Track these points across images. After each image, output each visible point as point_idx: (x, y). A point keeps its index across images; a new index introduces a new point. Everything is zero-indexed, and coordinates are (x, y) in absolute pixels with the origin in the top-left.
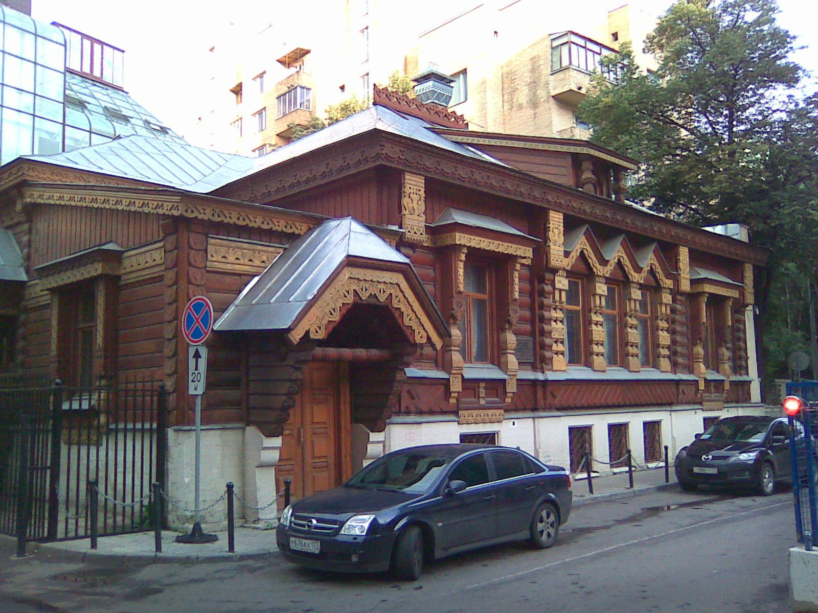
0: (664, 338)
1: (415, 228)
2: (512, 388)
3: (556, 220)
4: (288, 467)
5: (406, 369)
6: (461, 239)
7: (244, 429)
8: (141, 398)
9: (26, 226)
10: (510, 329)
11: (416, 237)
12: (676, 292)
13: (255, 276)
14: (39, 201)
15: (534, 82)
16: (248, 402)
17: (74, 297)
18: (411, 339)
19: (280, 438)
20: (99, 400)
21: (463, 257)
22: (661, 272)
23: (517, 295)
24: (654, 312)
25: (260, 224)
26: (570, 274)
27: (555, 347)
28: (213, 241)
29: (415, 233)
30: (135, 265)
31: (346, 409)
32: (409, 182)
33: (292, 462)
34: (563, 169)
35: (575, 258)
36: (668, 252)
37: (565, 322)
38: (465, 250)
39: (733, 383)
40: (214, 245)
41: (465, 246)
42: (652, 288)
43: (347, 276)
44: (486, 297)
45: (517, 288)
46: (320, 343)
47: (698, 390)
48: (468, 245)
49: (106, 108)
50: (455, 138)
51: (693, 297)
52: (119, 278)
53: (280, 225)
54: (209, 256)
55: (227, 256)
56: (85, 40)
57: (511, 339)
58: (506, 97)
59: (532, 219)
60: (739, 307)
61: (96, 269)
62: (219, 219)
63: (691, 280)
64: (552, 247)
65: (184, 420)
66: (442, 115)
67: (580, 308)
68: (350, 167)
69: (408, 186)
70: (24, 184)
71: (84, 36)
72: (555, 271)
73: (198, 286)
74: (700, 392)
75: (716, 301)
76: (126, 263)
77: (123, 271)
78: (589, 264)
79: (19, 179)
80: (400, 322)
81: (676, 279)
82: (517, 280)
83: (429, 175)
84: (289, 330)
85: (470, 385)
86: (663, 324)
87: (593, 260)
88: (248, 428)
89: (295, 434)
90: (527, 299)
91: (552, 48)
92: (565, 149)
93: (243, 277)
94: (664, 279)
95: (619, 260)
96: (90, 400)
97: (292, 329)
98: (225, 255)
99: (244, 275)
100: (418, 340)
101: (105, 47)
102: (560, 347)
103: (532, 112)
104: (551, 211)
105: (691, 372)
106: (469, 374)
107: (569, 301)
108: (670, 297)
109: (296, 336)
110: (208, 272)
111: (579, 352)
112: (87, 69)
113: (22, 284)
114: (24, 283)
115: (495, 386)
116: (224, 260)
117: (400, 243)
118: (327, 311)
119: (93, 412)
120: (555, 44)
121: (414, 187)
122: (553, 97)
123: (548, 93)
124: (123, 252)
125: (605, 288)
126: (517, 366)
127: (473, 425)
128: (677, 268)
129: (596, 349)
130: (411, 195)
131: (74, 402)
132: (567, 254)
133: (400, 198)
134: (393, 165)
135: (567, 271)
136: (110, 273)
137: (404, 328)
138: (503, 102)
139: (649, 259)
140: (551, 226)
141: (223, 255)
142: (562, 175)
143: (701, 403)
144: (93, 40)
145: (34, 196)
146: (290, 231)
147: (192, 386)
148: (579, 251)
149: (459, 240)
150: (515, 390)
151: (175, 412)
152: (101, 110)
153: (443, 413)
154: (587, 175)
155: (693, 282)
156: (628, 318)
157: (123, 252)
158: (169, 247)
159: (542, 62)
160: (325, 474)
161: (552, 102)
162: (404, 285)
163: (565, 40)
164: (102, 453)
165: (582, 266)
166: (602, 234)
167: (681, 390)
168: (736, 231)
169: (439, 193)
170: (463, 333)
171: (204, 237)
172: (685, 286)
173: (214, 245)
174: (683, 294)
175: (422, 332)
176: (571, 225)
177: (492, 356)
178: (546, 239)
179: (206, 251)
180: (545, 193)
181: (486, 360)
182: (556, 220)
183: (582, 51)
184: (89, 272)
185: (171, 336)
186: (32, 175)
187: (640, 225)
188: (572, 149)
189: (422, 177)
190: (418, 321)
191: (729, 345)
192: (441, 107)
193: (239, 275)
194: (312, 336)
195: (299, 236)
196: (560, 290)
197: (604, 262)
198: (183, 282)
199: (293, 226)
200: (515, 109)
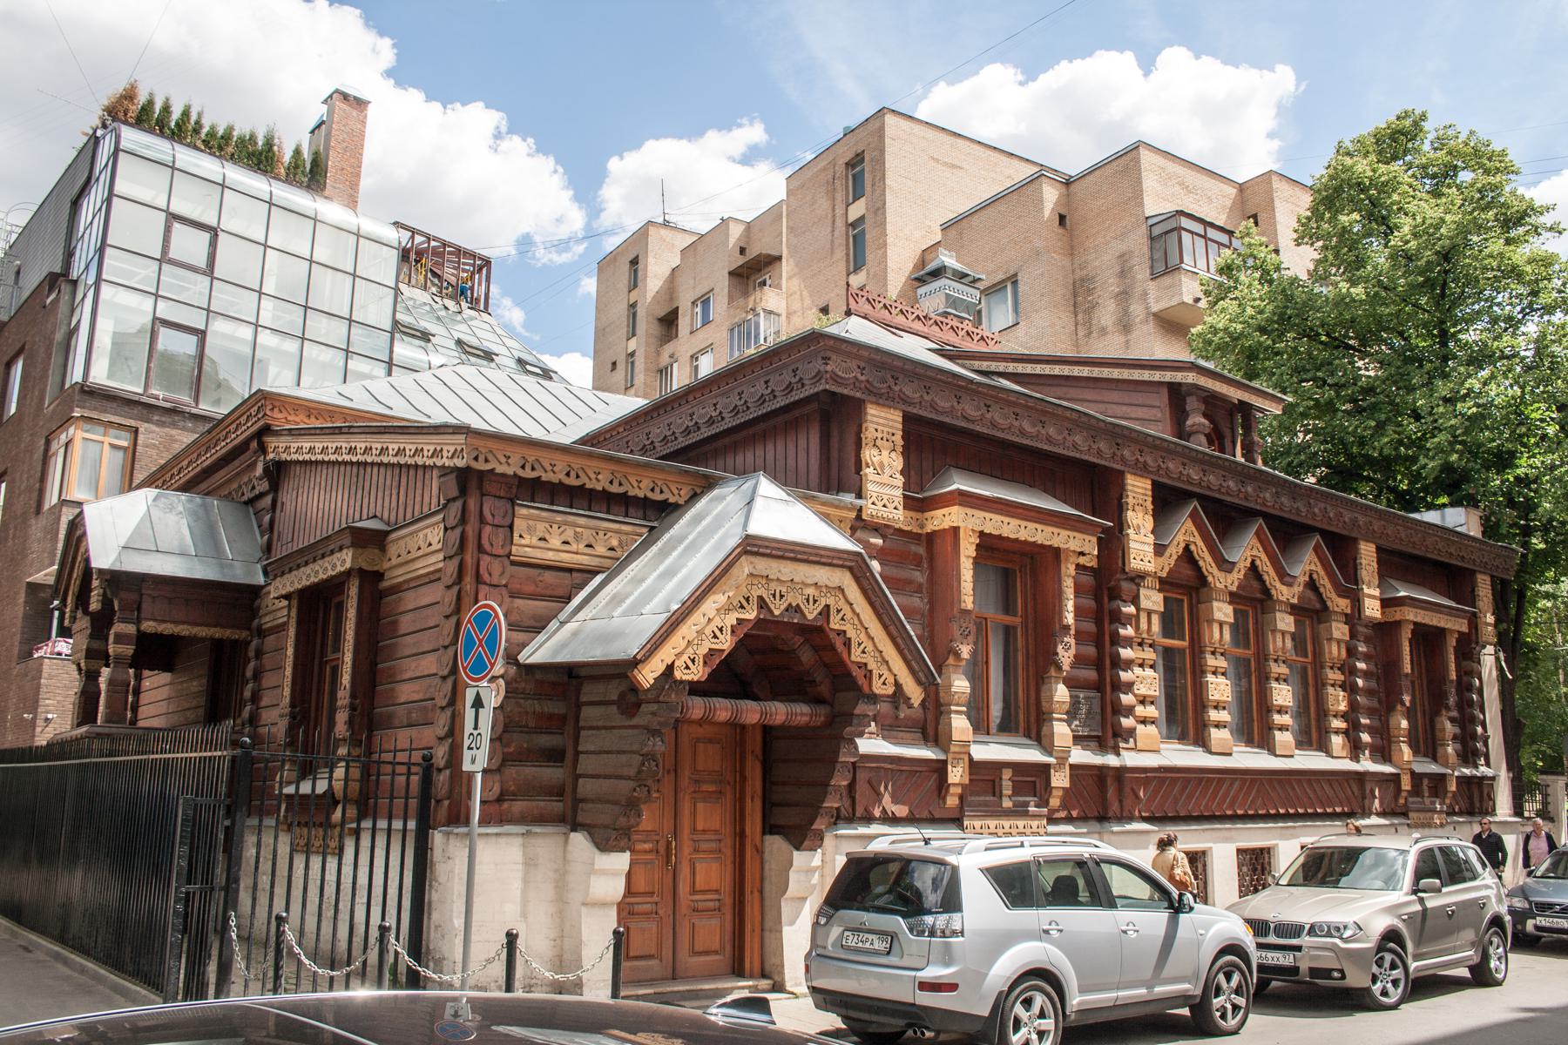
0: (1338, 701)
2: (1060, 780)
3: (1138, 489)
4: (647, 907)
5: (858, 741)
7: (566, 835)
8: (404, 778)
9: (268, 500)
12: (1354, 618)
13: (598, 573)
14: (284, 456)
15: (1125, 292)
17: (317, 605)
18: (866, 689)
19: (628, 854)
20: (346, 779)
22: (1329, 586)
23: (1070, 618)
24: (1318, 654)
26: (1165, 584)
27: (1140, 710)
28: (524, 511)
30: (404, 553)
31: (754, 810)
33: (655, 899)
34: (1154, 411)
35: (1175, 557)
36: (1340, 549)
37: (1160, 668)
39: (1464, 781)
40: (526, 518)
42: (1312, 612)
43: (746, 571)
44: (1016, 620)
46: (695, 689)
47: (1399, 790)
49: (459, 342)
50: (977, 364)
51: (1385, 631)
52: (379, 576)
53: (640, 488)
54: (516, 535)
58: (1080, 317)
59: (1094, 489)
60: (1468, 648)
61: (344, 560)
62: (534, 475)
63: (1382, 601)
65: (459, 817)
67: (1185, 644)
69: (871, 427)
74: (1404, 794)
75: (1428, 639)
76: (393, 550)
79: (261, 423)
80: (845, 655)
81: (1357, 601)
83: (909, 409)
84: (635, 663)
85: (985, 775)
86: (1335, 676)
88: (573, 835)
89: (662, 850)
90: (1091, 627)
91: (1152, 239)
92: (1157, 376)
93: (575, 575)
94: (1333, 596)
95: (1253, 562)
96: (330, 778)
97: (641, 661)
98: (542, 536)
100: (878, 688)
102: (1151, 711)
103: (1122, 339)
106: (981, 752)
107: (1168, 630)
109: (648, 675)
110: (513, 563)
111: (1186, 718)
113: (255, 591)
114: (262, 587)
115: (1032, 779)
116: (542, 544)
117: (859, 525)
118: (708, 631)
119: (329, 800)
120: (1157, 231)
121: (882, 424)
122: (1155, 315)
124: (387, 533)
125: (1229, 609)
128: (1356, 580)
129: (1214, 715)
130: (879, 442)
131: (319, 783)
132: (1159, 550)
134: (845, 392)
136: (366, 567)
139: (1307, 562)
142: (1153, 422)
143: (1405, 815)
145: (281, 449)
146: (659, 497)
147: (467, 755)
148: (1182, 545)
150: (1066, 784)
151: (446, 803)
152: (452, 344)
154: (1196, 420)
155: (1386, 603)
156: (1272, 664)
157: (387, 533)
158: (452, 522)
159: (1135, 260)
160: (715, 922)
161: (1151, 327)
162: (853, 592)
163: (1172, 224)
164: (347, 870)
165: (1187, 571)
166: (1224, 518)
168: (1459, 519)
169: (934, 446)
170: (973, 679)
171: (509, 506)
172: (1372, 609)
173: (526, 518)
175: (886, 674)
176: (1166, 501)
177: (1028, 722)
178: (1121, 525)
179: (511, 527)
181: (1017, 731)
182: (1138, 489)
183: (1200, 242)
184: (334, 566)
185: (445, 672)
186: (279, 419)
187: (1286, 506)
188: (1168, 376)
191: (1455, 714)
193: (570, 570)
194: (678, 675)
195: (676, 506)
196: (1149, 613)
197: (1225, 565)
198: (469, 580)
199: (665, 489)
200: (1095, 335)
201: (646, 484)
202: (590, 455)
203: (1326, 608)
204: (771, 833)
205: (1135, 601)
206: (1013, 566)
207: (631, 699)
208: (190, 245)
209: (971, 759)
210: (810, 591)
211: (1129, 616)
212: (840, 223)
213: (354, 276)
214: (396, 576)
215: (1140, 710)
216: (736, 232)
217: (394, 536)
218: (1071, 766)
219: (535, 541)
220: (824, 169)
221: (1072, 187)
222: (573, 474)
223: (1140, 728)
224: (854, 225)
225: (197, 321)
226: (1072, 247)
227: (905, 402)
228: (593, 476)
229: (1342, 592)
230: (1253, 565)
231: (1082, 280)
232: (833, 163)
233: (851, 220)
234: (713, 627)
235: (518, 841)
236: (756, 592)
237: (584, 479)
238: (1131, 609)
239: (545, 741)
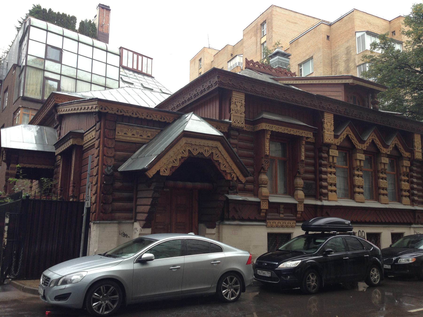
0: (405, 186)
1: (239, 120)
6: (264, 126)
7: (133, 223)
10: (300, 177)
11: (240, 125)
12: (412, 160)
13: (144, 144)
16: (136, 209)
21: (268, 136)
23: (303, 158)
25: (146, 117)
27: (330, 188)
28: (119, 125)
29: (238, 123)
32: (235, 96)
38: (270, 133)
41: (269, 130)
42: (396, 159)
43: (184, 142)
45: (303, 154)
46: (167, 178)
48: (271, 130)
52: (82, 146)
54: (117, 133)
55: (127, 133)
56: (135, 55)
57: (300, 182)
64: (326, 132)
66: (283, 73)
68: (205, 90)
70: (56, 106)
71: (134, 53)
72: (329, 146)
73: (110, 148)
77: (84, 143)
78: (352, 143)
80: (218, 168)
81: (412, 152)
82: (303, 150)
83: (247, 93)
85: (275, 207)
87: (355, 141)
88: (135, 223)
92: (340, 81)
94: (404, 152)
97: (149, 170)
99: (138, 143)
101: (144, 57)
104: (325, 113)
105: (256, 195)
106: (273, 199)
108: (409, 163)
109: (151, 174)
110: (116, 141)
112: (135, 67)
115: (291, 208)
116: (125, 135)
118: (171, 161)
123: (355, 64)
126: (303, 197)
127: (286, 228)
128: (413, 146)
130: (237, 103)
132: (336, 137)
133: (230, 105)
135: (337, 146)
136: (77, 144)
137: (221, 172)
138: (332, 71)
140: (326, 121)
141: (125, 132)
143: (264, 221)
144: (138, 54)
148: (345, 135)
149: (265, 127)
150: (267, 208)
153: (256, 220)
162: (221, 148)
166: (361, 128)
167: (417, 216)
174: (418, 161)
179: (115, 130)
180: (321, 103)
188: (344, 81)
189: (243, 94)
190: (230, 167)
192: (282, 69)
193: (135, 143)
194: (161, 174)
201: (158, 116)
202: (160, 111)
203: (401, 156)
204: (201, 223)
205: (328, 153)
206: (289, 143)
207: (148, 181)
208: (54, 54)
209: (269, 202)
210: (207, 148)
211: (326, 158)
212: (259, 44)
213: (92, 59)
214: (86, 146)
215: (330, 188)
216: (230, 48)
217: (85, 134)
218: (304, 204)
219: (123, 134)
220: (254, 27)
221: (332, 27)
222: (134, 114)
223: (330, 193)
224: (263, 44)
225: (57, 77)
226: (331, 46)
227: (245, 90)
228: (141, 114)
229: (407, 151)
230: (373, 141)
231: (334, 57)
232: (257, 25)
233: (262, 42)
234: (173, 159)
235: (117, 225)
236: (187, 149)
237: (138, 115)
238: (325, 155)
239: (125, 194)
